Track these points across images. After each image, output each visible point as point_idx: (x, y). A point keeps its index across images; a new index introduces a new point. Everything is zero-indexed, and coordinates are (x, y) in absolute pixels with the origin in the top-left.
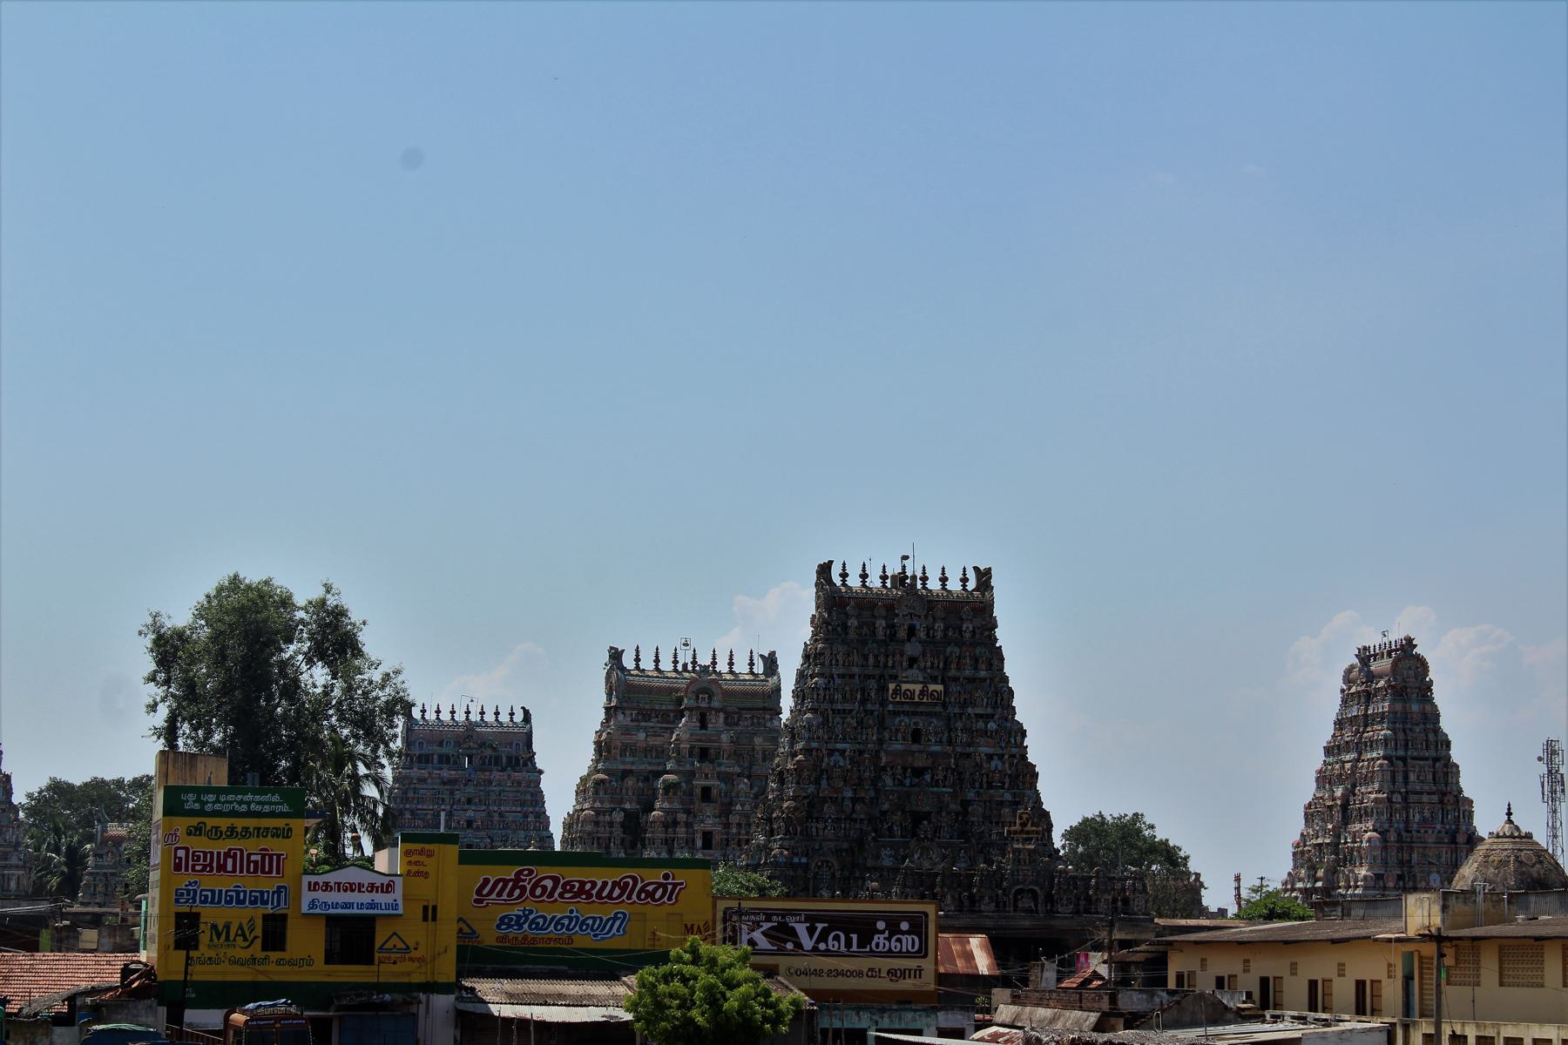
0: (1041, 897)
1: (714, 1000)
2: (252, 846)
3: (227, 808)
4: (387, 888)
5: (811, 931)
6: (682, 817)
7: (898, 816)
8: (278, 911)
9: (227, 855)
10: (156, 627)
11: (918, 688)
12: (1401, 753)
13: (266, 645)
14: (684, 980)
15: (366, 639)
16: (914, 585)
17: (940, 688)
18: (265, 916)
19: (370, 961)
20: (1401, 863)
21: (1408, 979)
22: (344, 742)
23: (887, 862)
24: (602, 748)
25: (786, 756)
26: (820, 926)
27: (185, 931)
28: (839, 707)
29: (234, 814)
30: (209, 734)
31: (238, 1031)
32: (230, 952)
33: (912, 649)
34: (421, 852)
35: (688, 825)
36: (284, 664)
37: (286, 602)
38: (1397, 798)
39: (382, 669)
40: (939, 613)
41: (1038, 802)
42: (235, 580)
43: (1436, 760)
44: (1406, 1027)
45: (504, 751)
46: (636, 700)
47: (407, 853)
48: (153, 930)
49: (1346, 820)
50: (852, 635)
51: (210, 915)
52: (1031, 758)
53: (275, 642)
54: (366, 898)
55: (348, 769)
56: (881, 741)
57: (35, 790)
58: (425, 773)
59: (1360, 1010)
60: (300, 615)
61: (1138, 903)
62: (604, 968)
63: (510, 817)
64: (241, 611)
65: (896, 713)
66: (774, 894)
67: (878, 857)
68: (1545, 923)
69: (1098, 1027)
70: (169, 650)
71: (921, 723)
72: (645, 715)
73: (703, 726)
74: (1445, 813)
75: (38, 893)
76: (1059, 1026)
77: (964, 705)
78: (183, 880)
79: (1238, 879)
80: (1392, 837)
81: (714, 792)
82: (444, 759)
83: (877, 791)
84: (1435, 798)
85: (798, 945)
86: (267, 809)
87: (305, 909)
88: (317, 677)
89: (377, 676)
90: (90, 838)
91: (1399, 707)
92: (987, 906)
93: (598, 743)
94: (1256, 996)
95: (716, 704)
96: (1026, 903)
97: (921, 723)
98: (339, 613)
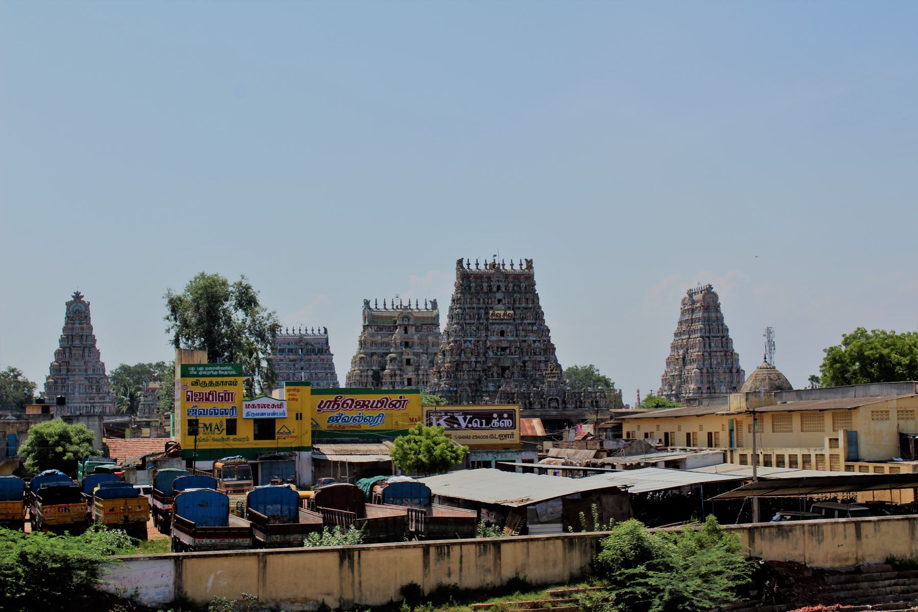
0: (560, 402)
1: (429, 450)
2: (220, 389)
3: (209, 373)
4: (280, 406)
5: (465, 419)
6: (398, 372)
7: (495, 369)
8: (233, 418)
9: (209, 394)
10: (169, 294)
11: (502, 312)
12: (707, 334)
13: (216, 302)
14: (416, 442)
15: (260, 299)
16: (499, 268)
17: (512, 312)
18: (227, 420)
19: (274, 439)
20: (709, 382)
21: (731, 431)
22: (252, 344)
23: (491, 389)
24: (362, 344)
25: (445, 344)
26: (469, 417)
27: (193, 427)
28: (468, 321)
29: (212, 376)
30: (193, 342)
31: (219, 471)
32: (213, 436)
33: (499, 295)
34: (294, 390)
35: (401, 375)
36: (225, 311)
37: (224, 284)
38: (706, 354)
39: (268, 311)
40: (511, 279)
41: (556, 360)
42: (203, 276)
43: (723, 337)
44: (732, 451)
45: (316, 347)
46: (377, 323)
47: (288, 391)
48: (178, 427)
49: (684, 364)
50: (473, 290)
51: (203, 420)
52: (552, 342)
53: (220, 301)
54: (271, 410)
55: (255, 355)
56: (487, 336)
57: (113, 369)
58: (282, 357)
59: (710, 445)
60: (231, 289)
61: (602, 403)
62: (375, 438)
63: (320, 375)
64: (205, 288)
65: (493, 324)
66: (442, 404)
67: (487, 386)
68: (791, 404)
69: (596, 457)
70: (175, 305)
71: (504, 327)
72: (380, 328)
73: (406, 332)
74: (727, 360)
75: (118, 413)
76: (578, 456)
77: (522, 319)
78: (190, 405)
79: (638, 391)
80: (705, 371)
81: (412, 361)
82: (291, 351)
83: (486, 358)
84: (723, 354)
85: (459, 424)
86: (226, 373)
87: (244, 416)
88: (238, 316)
89: (265, 315)
90: (140, 389)
91: (706, 315)
92: (537, 406)
93: (360, 341)
94: (663, 441)
95: (411, 322)
96: (554, 404)
97: (504, 327)
98: (248, 288)
